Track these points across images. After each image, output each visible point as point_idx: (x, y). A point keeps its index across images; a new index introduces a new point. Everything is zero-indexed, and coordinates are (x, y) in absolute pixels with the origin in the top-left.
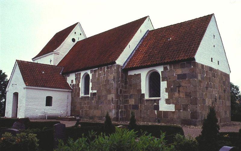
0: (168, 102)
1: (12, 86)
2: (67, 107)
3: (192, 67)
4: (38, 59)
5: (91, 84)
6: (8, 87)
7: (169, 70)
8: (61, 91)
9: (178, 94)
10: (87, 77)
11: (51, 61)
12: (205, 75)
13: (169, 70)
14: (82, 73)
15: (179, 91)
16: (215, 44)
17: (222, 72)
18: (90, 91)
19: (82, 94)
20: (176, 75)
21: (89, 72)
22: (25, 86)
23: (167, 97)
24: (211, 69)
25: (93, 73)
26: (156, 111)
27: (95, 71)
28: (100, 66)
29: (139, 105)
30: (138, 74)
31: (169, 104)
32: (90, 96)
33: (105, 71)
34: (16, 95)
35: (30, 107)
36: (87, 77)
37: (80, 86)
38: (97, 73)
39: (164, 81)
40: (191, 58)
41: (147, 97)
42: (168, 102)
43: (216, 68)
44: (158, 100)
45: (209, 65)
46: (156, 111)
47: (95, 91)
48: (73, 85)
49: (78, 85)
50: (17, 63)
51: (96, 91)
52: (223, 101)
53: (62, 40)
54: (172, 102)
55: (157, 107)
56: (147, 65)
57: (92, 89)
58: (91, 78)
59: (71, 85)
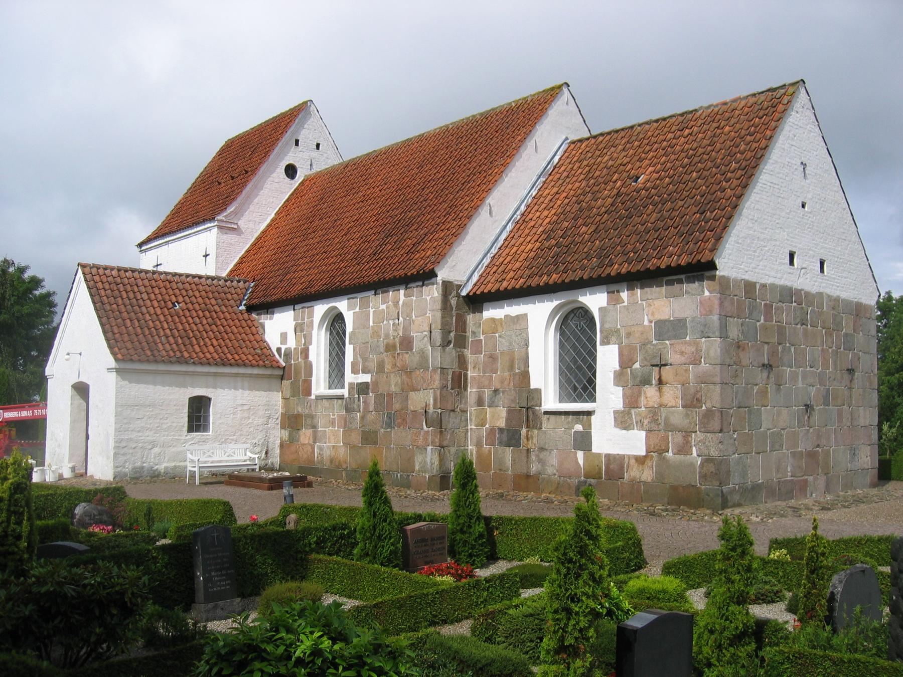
0: (623, 421)
1: (67, 360)
2: (223, 475)
3: (707, 293)
4: (160, 245)
5: (349, 350)
6: (54, 362)
7: (626, 304)
8: (251, 376)
9: (658, 394)
10: (336, 322)
11: (206, 256)
12: (762, 321)
13: (626, 304)
14: (320, 309)
15: (660, 382)
16: (808, 198)
17: (837, 300)
18: (350, 377)
19: (320, 385)
20: (651, 322)
21: (342, 305)
22: (111, 362)
23: (619, 405)
24: (789, 295)
25: (357, 309)
26: (580, 455)
27: (365, 305)
28: (381, 285)
29: (524, 431)
30: (518, 317)
31: (626, 428)
32: (346, 395)
33: (401, 303)
34: (82, 390)
35: (133, 435)
36: (336, 322)
37: (312, 357)
38: (371, 311)
39: (608, 343)
40: (699, 261)
41: (550, 401)
42: (623, 421)
43: (814, 290)
44: (589, 413)
45: (782, 282)
46: (580, 455)
47: (366, 378)
48: (288, 355)
49: (305, 352)
50: (80, 272)
51: (369, 375)
52: (840, 414)
53: (247, 172)
54: (637, 422)
55: (584, 441)
56: (547, 284)
57: (355, 371)
58: (349, 328)
59: (279, 350)
